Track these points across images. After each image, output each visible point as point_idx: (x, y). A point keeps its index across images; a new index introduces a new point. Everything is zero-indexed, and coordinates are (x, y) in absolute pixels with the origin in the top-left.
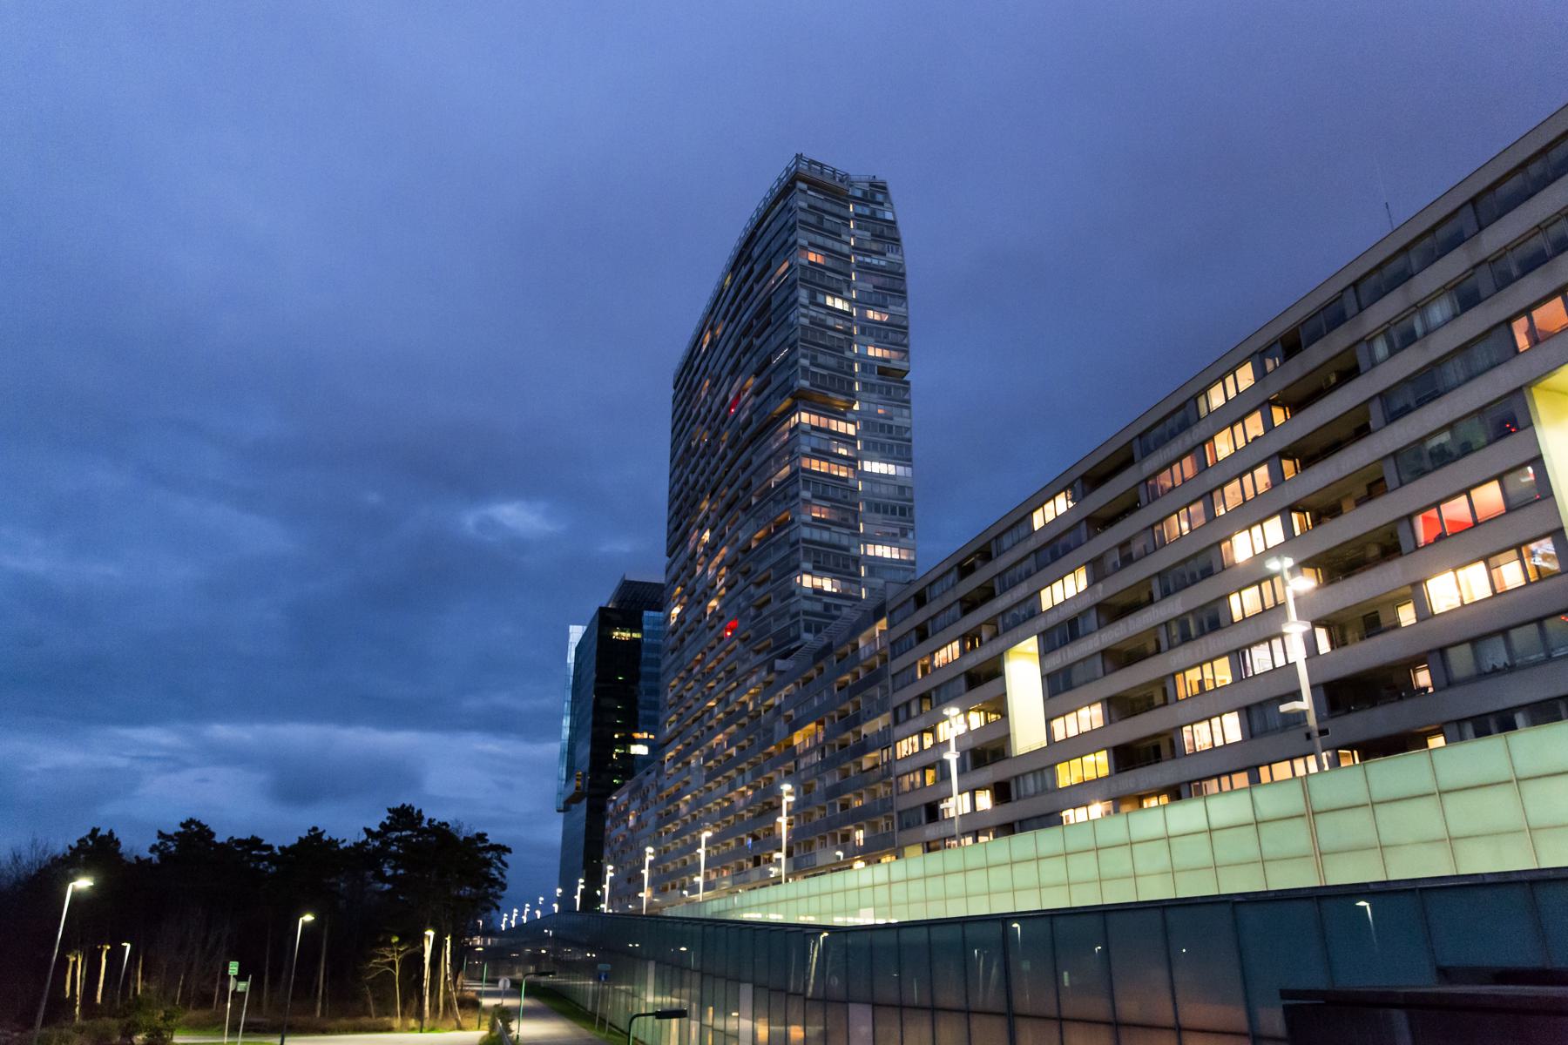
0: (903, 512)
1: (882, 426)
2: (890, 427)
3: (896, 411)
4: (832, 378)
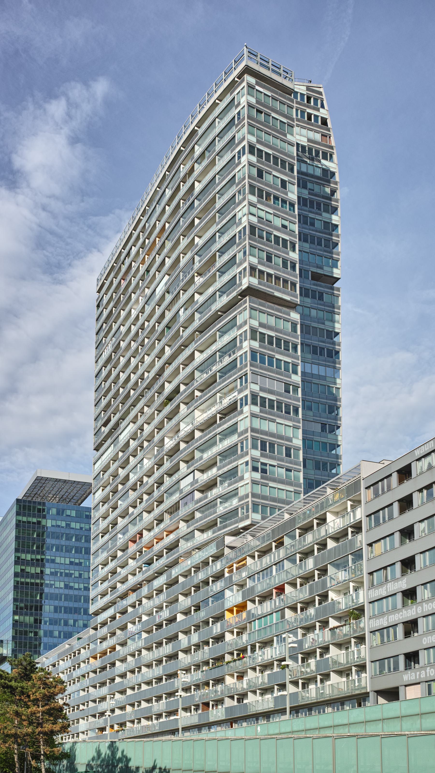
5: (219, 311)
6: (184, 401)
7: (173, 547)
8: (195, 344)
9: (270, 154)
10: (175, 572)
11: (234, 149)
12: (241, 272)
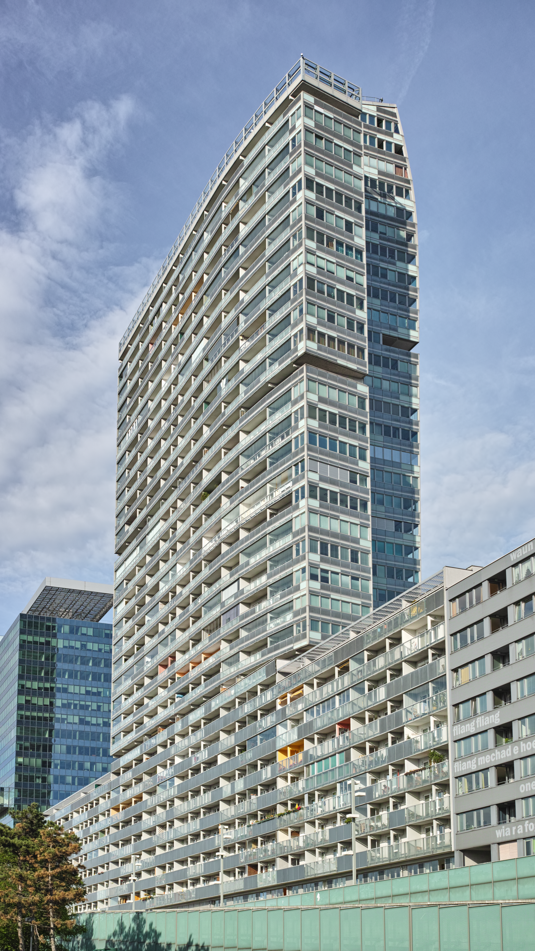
5: (269, 382)
7: (212, 673)
8: (240, 423)
9: (333, 190)
10: (215, 703)
11: (288, 184)
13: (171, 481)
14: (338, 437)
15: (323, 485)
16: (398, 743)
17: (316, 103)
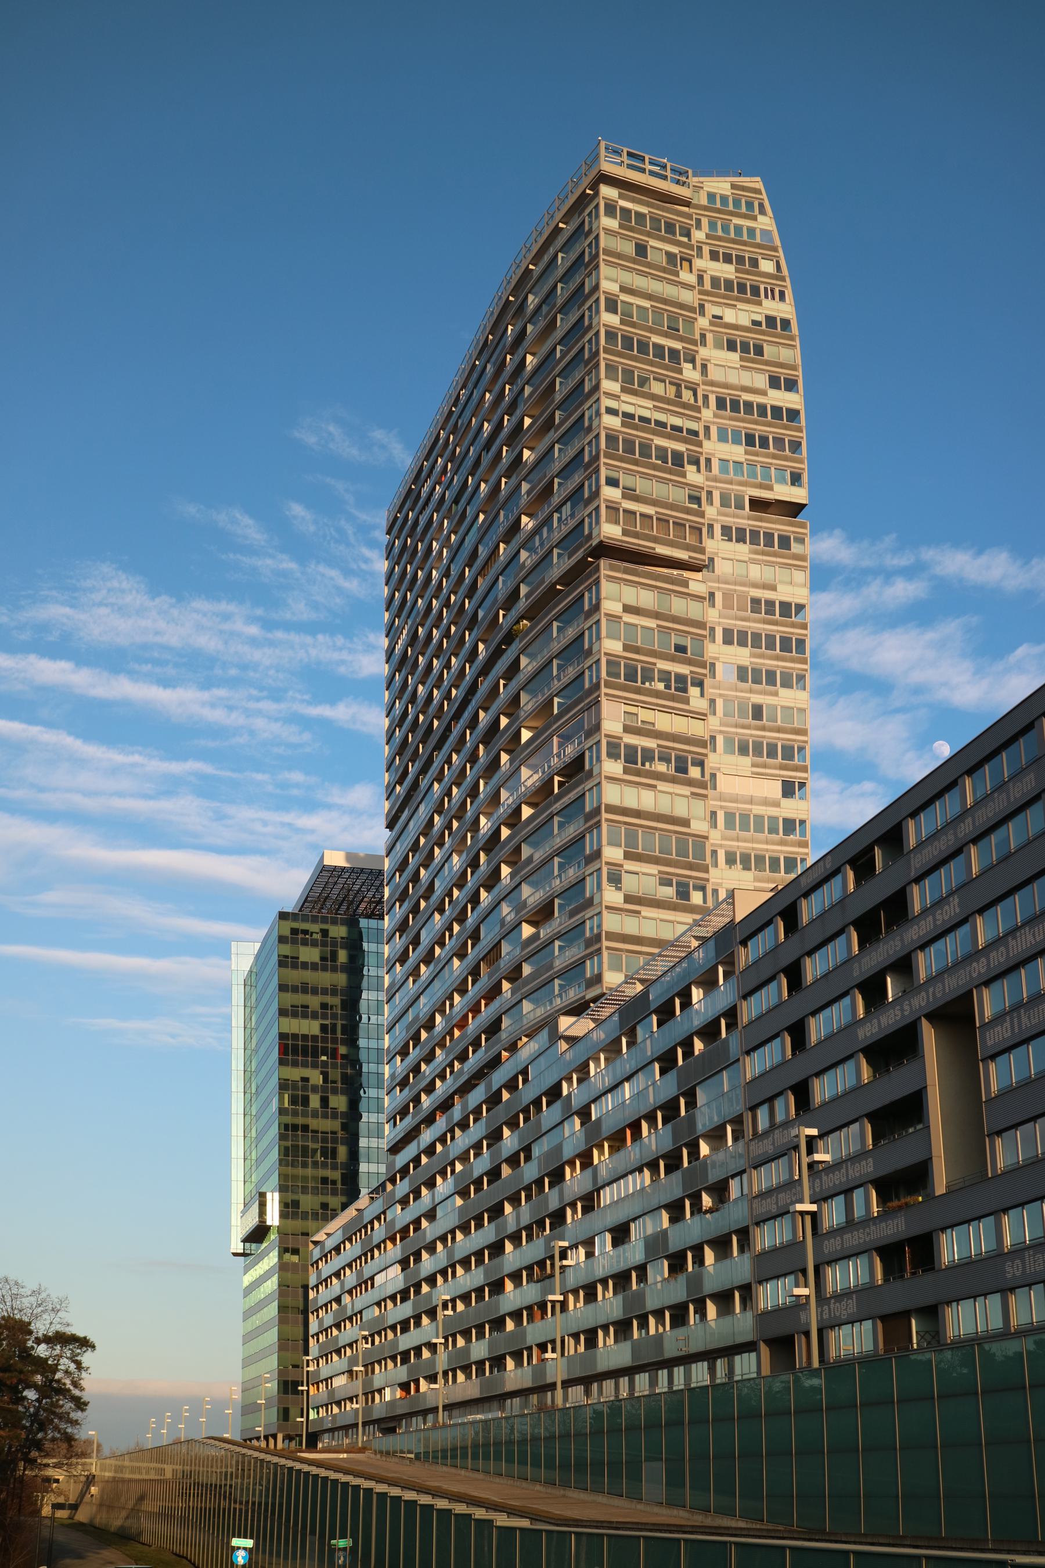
0: (788, 752)
1: (756, 601)
2: (770, 603)
3: (782, 574)
4: (663, 521)
5: (556, 583)
6: (507, 711)
7: (493, 1028)
8: (520, 642)
9: (648, 309)
10: (498, 1077)
11: (583, 304)
12: (590, 514)
13: (446, 719)
14: (655, 664)
15: (630, 739)
16: (693, 1163)
17: (621, 196)
